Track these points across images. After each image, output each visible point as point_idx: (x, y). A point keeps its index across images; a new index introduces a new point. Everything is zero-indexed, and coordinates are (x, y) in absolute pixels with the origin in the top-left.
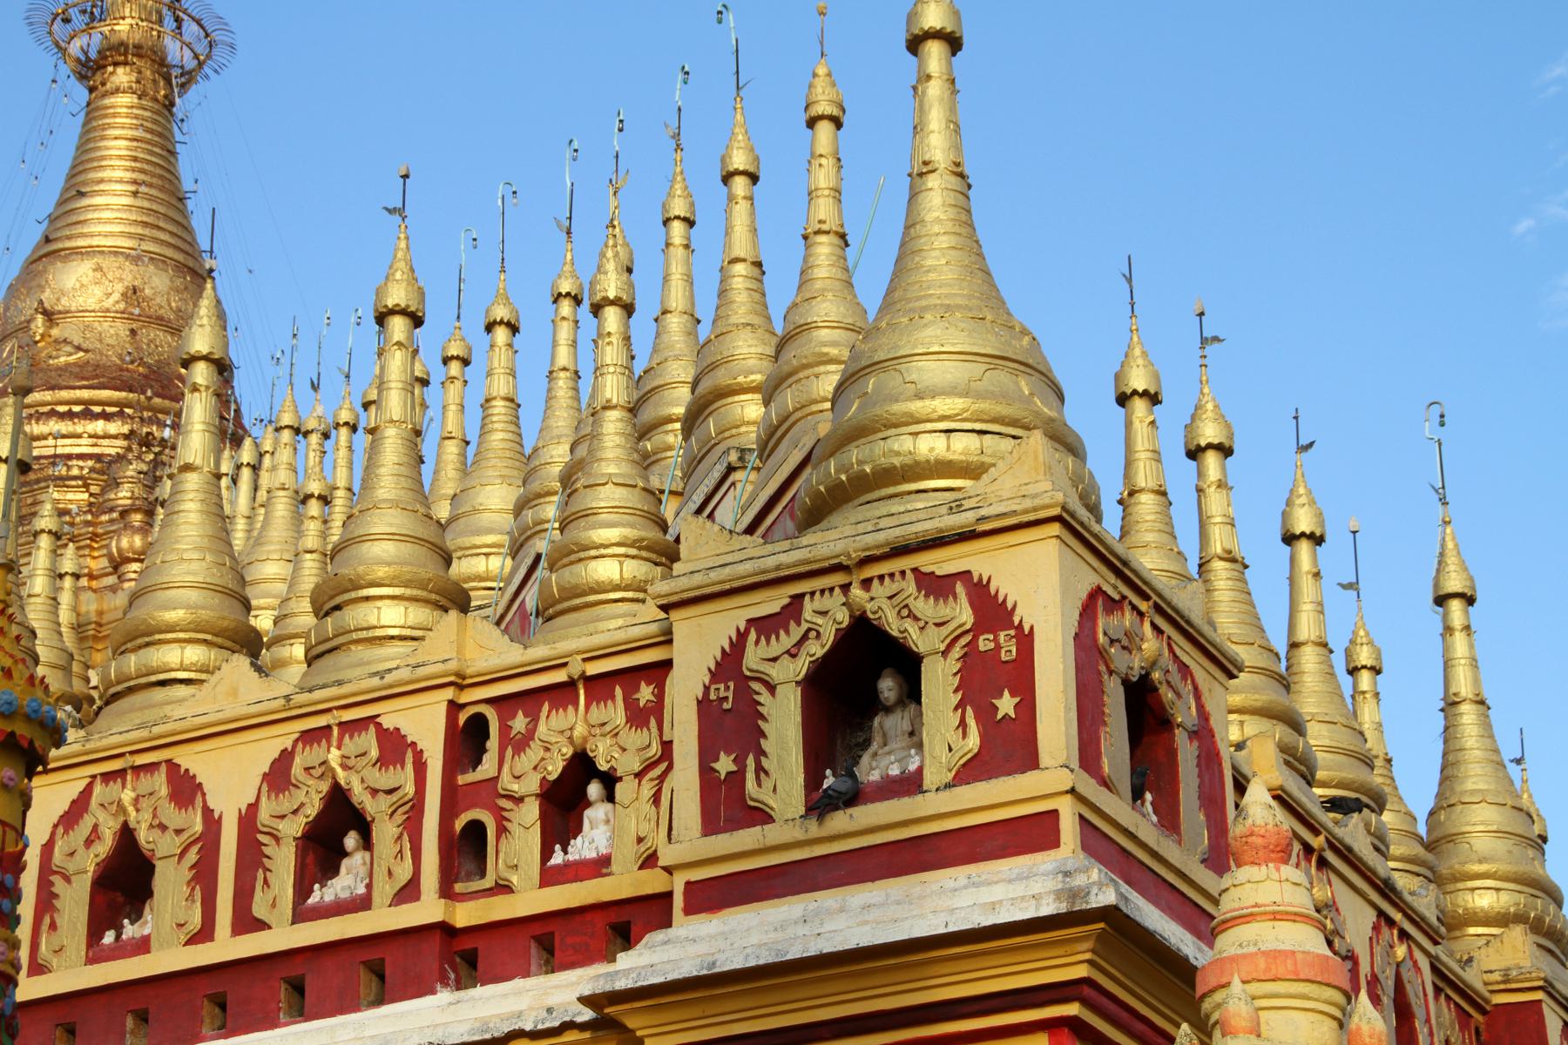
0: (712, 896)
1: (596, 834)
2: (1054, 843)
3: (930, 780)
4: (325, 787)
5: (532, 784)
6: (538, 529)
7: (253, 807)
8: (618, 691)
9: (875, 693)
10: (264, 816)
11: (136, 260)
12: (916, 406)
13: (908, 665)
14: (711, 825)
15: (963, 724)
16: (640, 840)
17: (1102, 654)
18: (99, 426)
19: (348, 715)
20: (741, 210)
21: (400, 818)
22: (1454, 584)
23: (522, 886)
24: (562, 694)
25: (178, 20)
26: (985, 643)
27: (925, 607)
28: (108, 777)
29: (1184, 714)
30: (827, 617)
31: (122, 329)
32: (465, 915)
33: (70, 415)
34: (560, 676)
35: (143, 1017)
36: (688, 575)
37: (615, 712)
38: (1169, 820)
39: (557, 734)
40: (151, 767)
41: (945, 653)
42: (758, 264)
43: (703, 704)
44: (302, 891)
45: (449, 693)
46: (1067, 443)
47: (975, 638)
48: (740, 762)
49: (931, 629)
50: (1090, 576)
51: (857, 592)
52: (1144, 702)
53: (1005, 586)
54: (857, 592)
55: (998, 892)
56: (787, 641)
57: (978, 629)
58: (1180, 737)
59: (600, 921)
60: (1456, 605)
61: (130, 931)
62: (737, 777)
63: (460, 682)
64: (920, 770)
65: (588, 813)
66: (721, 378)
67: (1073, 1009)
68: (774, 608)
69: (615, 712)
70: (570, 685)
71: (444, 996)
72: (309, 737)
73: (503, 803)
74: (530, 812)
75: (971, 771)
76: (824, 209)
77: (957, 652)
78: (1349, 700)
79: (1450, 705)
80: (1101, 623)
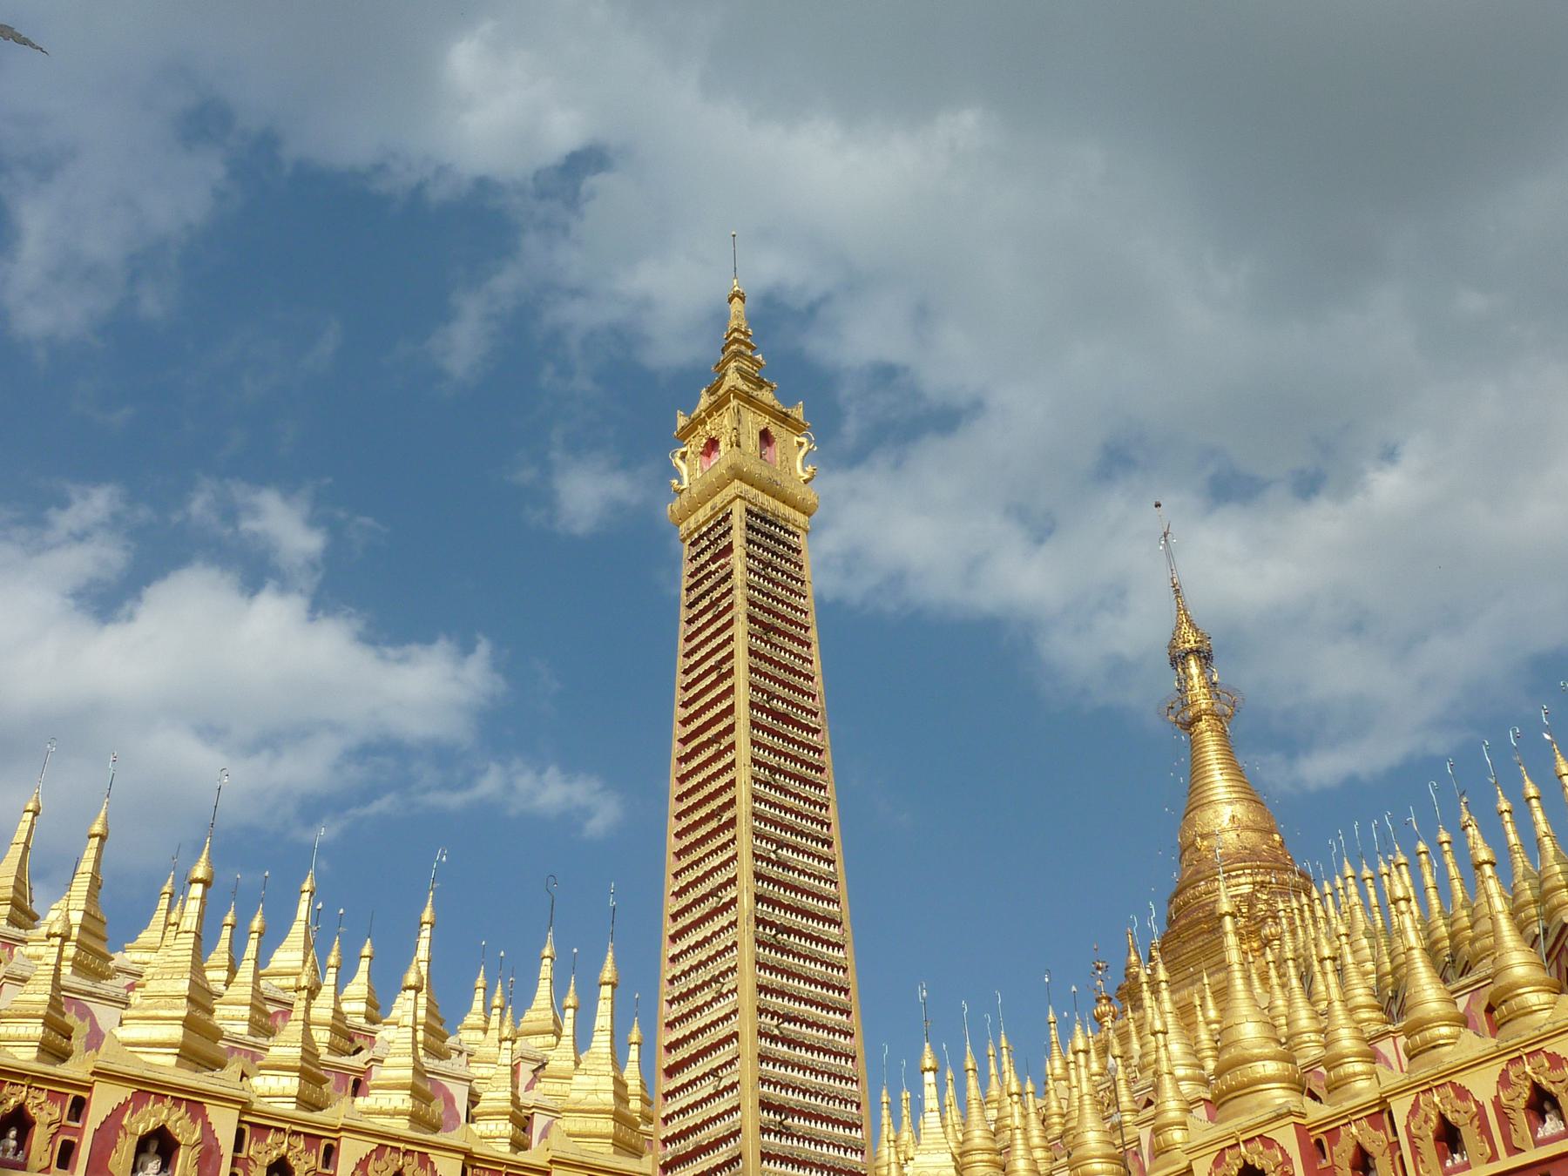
7: (1498, 1097)
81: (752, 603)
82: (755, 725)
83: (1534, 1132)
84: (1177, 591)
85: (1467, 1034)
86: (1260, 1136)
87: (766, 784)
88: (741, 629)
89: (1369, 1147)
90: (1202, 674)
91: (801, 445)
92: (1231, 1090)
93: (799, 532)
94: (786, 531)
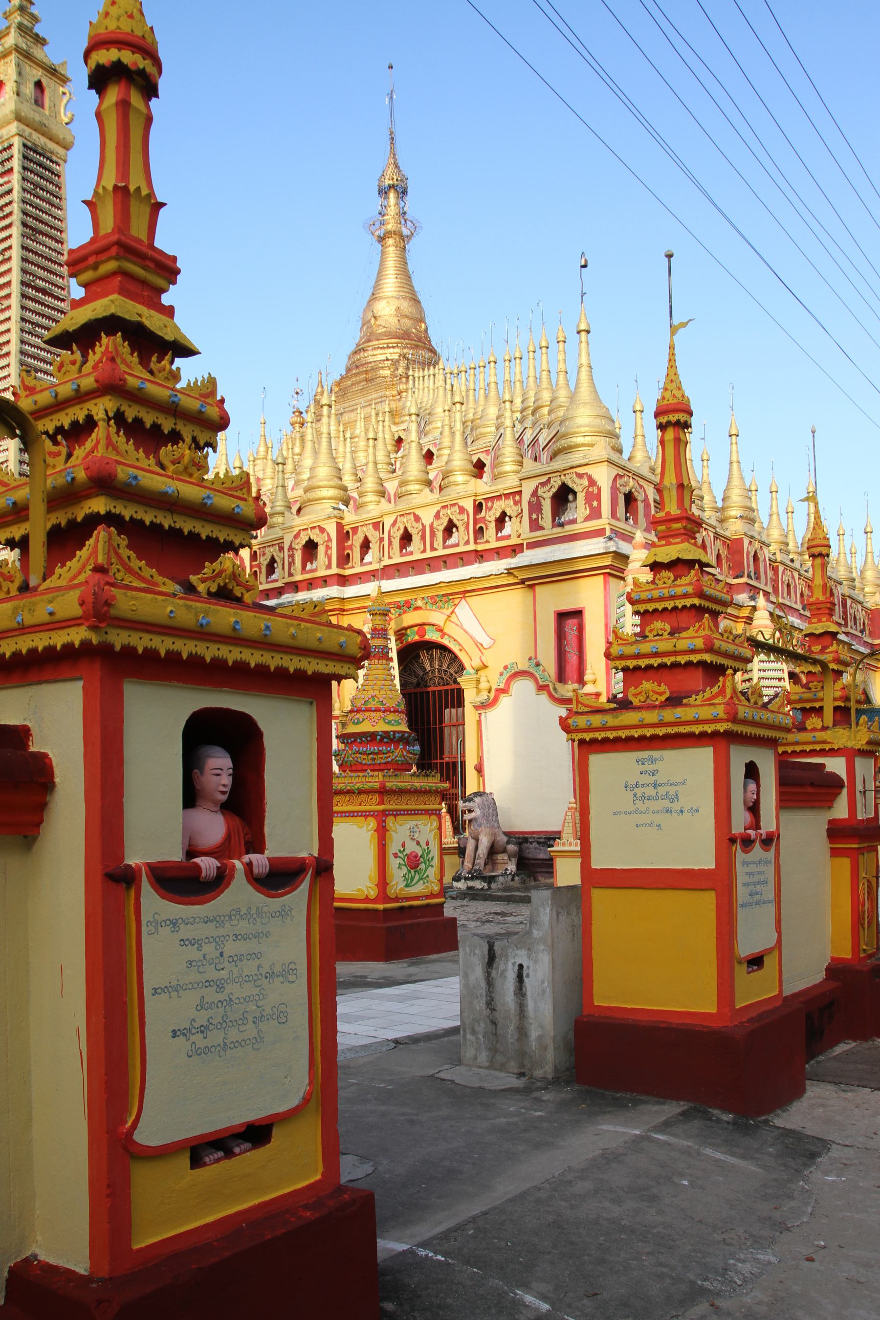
0: (533, 545)
1: (508, 529)
3: (578, 521)
5: (493, 519)
7: (432, 523)
10: (435, 525)
11: (398, 299)
12: (577, 430)
17: (618, 489)
18: (391, 350)
20: (544, 356)
22: (733, 432)
23: (490, 540)
24: (499, 497)
26: (591, 489)
27: (577, 480)
31: (396, 320)
32: (480, 548)
33: (383, 348)
34: (498, 494)
35: (413, 568)
37: (511, 502)
39: (498, 507)
40: (409, 514)
43: (529, 502)
44: (444, 542)
48: (537, 515)
51: (562, 477)
53: (595, 477)
54: (562, 477)
55: (592, 547)
56: (547, 488)
57: (590, 486)
58: (639, 503)
59: (509, 549)
60: (734, 437)
61: (409, 549)
62: (537, 519)
66: (540, 403)
67: (608, 571)
69: (511, 502)
70: (501, 495)
71: (476, 565)
72: (444, 507)
75: (588, 519)
76: (561, 366)
79: (731, 463)
81: (25, 213)
82: (24, 296)
83: (362, 559)
84: (392, 139)
85: (427, 490)
86: (319, 526)
87: (29, 333)
88: (16, 231)
89: (370, 538)
90: (397, 204)
91: (64, 94)
92: (310, 501)
93: (60, 162)
94: (52, 161)
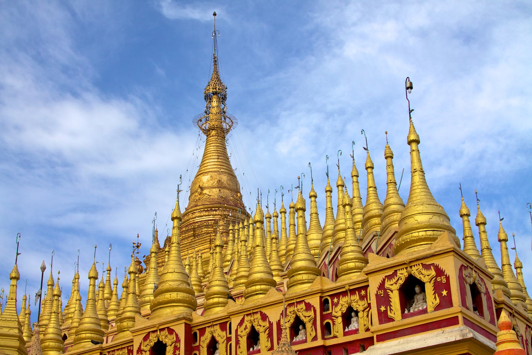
2: (457, 323)
4: (294, 316)
5: (339, 314)
6: (326, 245)
7: (279, 321)
8: (357, 292)
9: (415, 291)
10: (282, 323)
13: (422, 285)
14: (381, 322)
15: (435, 297)
16: (365, 325)
19: (298, 300)
21: (311, 322)
25: (225, 119)
26: (439, 279)
27: (424, 272)
28: (248, 315)
29: (483, 290)
30: (403, 274)
33: (208, 211)
34: (344, 290)
36: (371, 266)
37: (356, 297)
38: (481, 314)
41: (430, 282)
42: (375, 188)
43: (377, 295)
45: (320, 295)
46: (452, 231)
47: (436, 278)
48: (386, 308)
49: (426, 277)
50: (460, 262)
51: (409, 269)
52: (474, 288)
53: (442, 266)
54: (409, 269)
57: (437, 276)
58: (483, 295)
62: (386, 311)
63: (322, 292)
64: (427, 308)
65: (352, 319)
68: (391, 273)
73: (333, 318)
74: (340, 320)
75: (438, 308)
77: (432, 282)
78: (516, 275)
80: (464, 272)
